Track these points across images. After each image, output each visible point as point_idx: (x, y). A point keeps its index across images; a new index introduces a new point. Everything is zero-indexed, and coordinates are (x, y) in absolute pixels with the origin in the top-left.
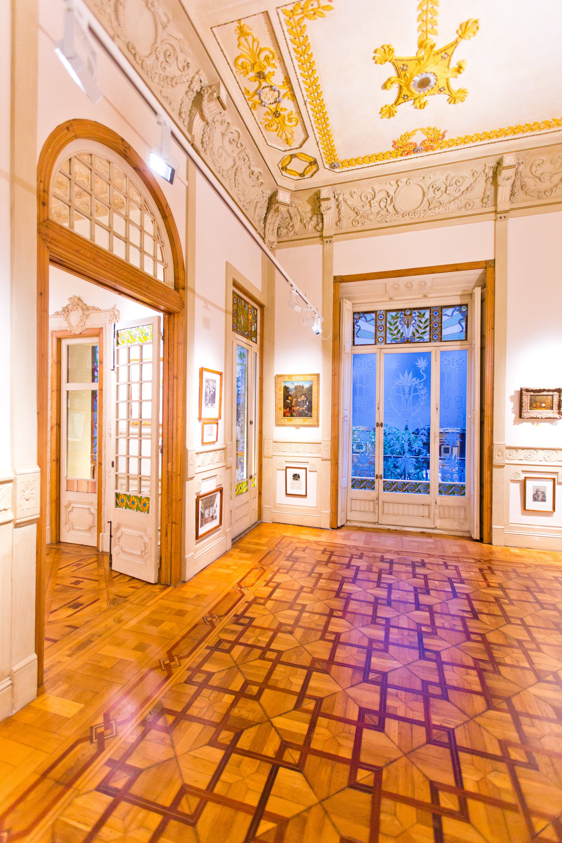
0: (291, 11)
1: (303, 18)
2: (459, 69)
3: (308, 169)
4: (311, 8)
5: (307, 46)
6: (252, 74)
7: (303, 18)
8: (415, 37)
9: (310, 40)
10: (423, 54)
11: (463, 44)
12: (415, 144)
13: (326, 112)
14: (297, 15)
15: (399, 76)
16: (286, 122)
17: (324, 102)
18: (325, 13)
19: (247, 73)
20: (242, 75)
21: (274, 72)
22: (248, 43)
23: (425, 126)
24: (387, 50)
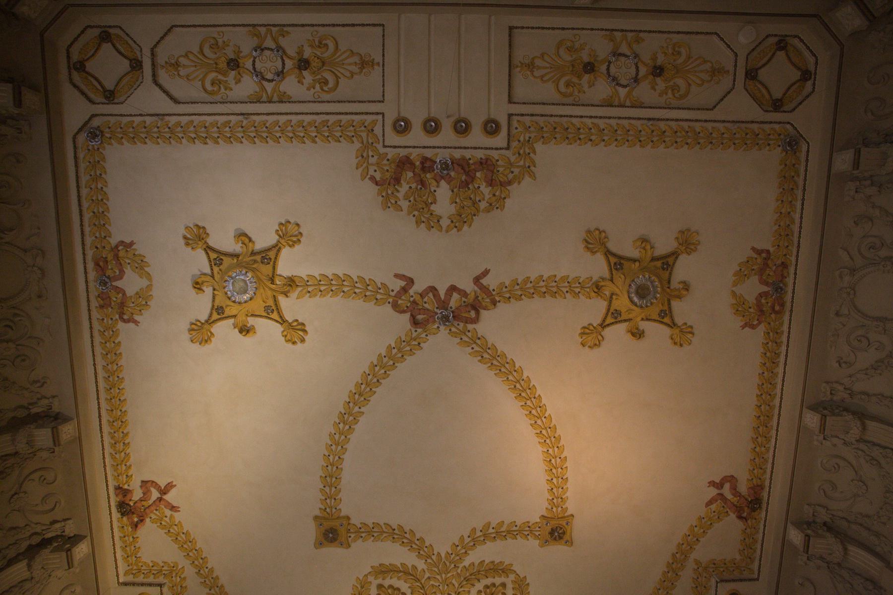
0: (372, 130)
1: (362, 143)
2: (245, 330)
3: (125, 81)
4: (371, 153)
5: (229, 140)
6: (307, 53)
7: (362, 143)
8: (302, 272)
9: (334, 144)
10: (278, 283)
11: (278, 329)
12: (120, 277)
13: (218, 143)
14: (368, 135)
15: (253, 253)
16: (213, 75)
17: (333, 144)
18: (361, 170)
19: (311, 46)
20: (311, 38)
21: (655, 90)
22: (350, 64)
23: (154, 292)
24: (295, 239)
